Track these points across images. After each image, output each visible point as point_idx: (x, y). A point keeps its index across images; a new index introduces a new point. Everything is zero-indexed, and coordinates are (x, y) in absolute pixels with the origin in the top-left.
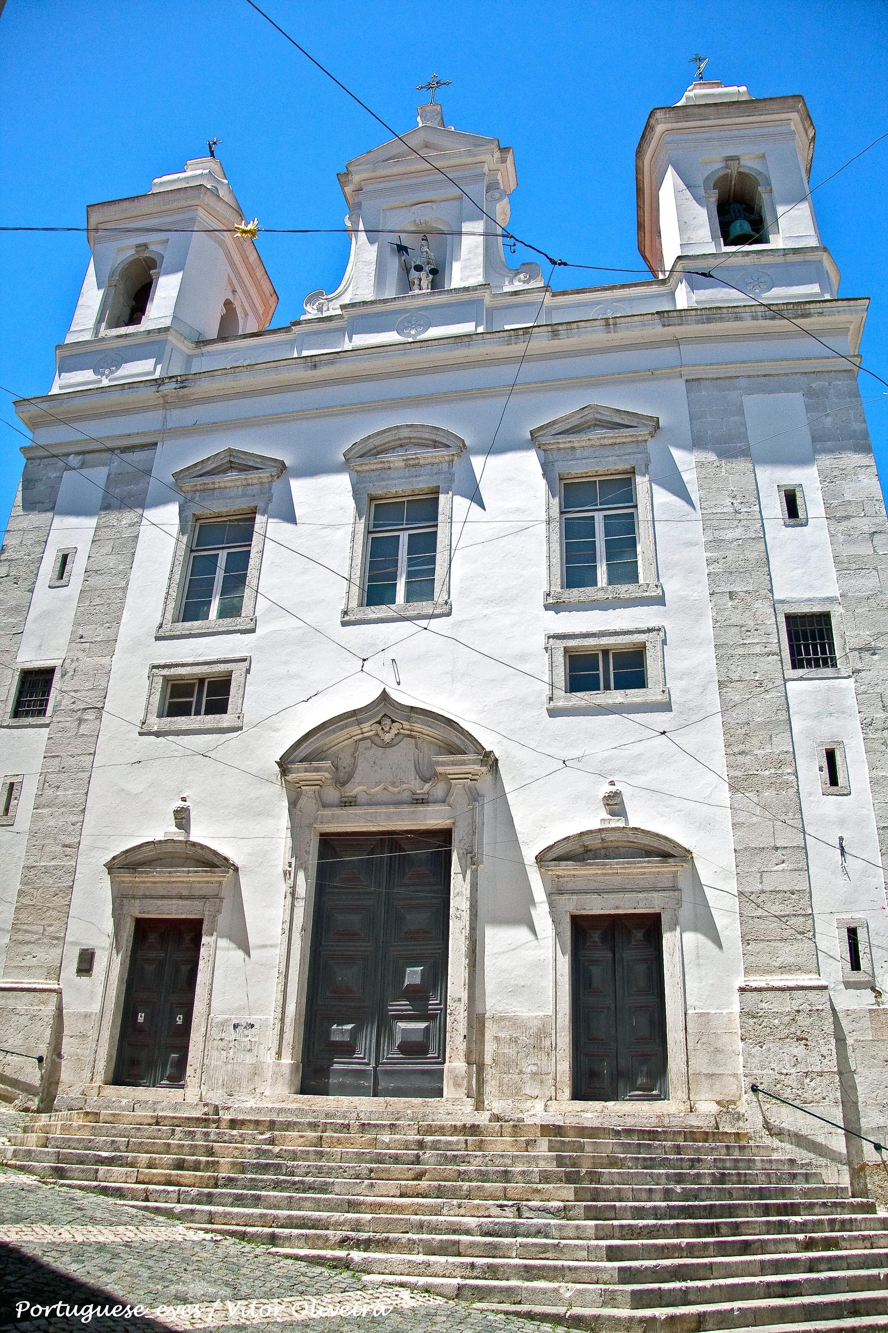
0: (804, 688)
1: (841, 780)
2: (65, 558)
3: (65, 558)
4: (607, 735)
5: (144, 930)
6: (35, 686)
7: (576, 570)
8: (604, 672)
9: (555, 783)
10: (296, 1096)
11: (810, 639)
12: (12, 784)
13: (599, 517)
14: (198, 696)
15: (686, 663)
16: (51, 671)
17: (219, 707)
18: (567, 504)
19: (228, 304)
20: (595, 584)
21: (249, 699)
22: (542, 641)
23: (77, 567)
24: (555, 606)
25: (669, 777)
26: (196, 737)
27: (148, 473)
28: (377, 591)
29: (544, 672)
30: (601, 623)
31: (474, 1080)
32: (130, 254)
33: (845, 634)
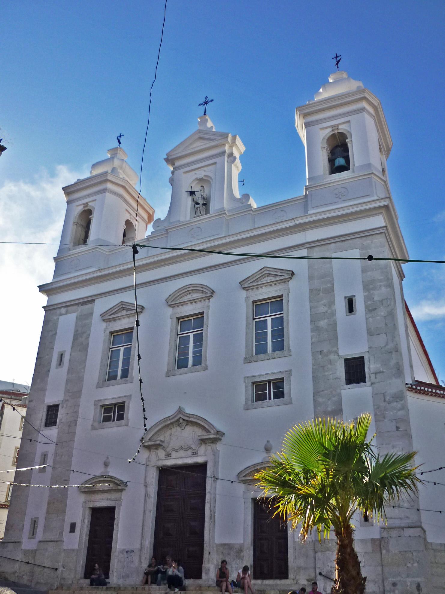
2: (62, 355)
3: (60, 364)
8: (271, 390)
13: (269, 320)
17: (121, 417)
26: (113, 429)
29: (243, 393)
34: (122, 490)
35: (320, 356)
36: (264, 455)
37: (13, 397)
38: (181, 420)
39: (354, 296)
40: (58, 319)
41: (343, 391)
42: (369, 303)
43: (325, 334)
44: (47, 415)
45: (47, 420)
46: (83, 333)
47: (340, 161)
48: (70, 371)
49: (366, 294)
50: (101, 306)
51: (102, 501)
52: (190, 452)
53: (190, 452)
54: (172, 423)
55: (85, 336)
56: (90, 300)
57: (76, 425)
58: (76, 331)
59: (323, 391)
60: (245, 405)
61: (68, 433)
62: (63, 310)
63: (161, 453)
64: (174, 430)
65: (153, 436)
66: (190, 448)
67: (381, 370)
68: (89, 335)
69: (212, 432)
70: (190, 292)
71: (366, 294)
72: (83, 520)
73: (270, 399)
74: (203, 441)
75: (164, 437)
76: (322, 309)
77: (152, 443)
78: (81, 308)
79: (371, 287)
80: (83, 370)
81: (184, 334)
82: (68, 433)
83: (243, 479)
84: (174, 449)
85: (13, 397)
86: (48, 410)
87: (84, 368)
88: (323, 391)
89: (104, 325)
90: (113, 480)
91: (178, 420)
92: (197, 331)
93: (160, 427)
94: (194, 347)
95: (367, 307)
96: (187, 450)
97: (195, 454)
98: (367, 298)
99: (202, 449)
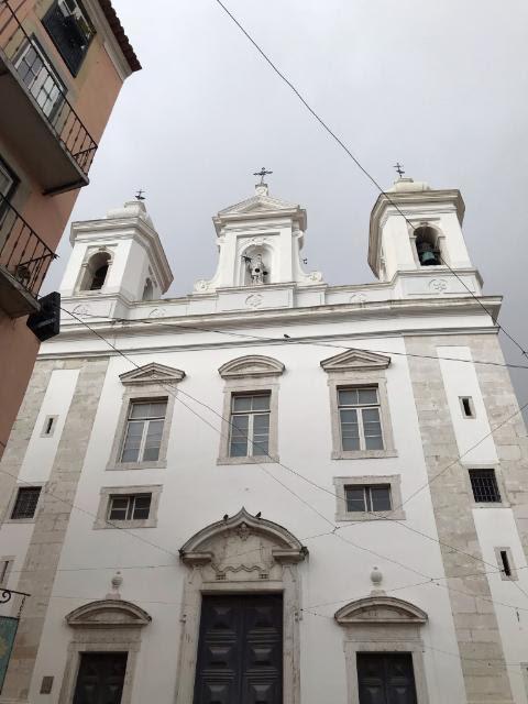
0: (483, 513)
1: (512, 572)
2: (51, 420)
3: (51, 420)
4: (370, 530)
5: (88, 659)
6: (26, 501)
7: (348, 441)
8: (369, 498)
9: (343, 566)
10: (91, 292)
11: (484, 485)
12: (7, 562)
13: (359, 411)
14: (131, 506)
15: (414, 495)
16: (39, 489)
18: (341, 400)
19: (148, 280)
20: (358, 449)
21: (161, 509)
22: (331, 480)
23: (58, 427)
24: (336, 457)
25: (401, 558)
26: (128, 535)
27: (104, 373)
28: (236, 448)
30: (365, 469)
31: (208, 536)
32: (96, 251)
33: (505, 482)
34: (142, 625)
35: (437, 463)
36: (373, 588)
37: (388, 307)
38: (244, 526)
39: (96, 527)
40: (51, 374)
41: (474, 510)
42: (491, 407)
43: (439, 440)
44: (17, 502)
45: (15, 508)
46: (87, 396)
47: (428, 256)
48: (64, 442)
49: (485, 396)
50: (120, 365)
51: (106, 643)
52: (255, 575)
53: (255, 575)
54: (229, 530)
55: (90, 400)
56: (104, 356)
57: (67, 519)
58: (78, 392)
59: (447, 506)
60: (337, 514)
61: (52, 530)
62: (60, 364)
63: (210, 574)
64: (230, 540)
65: (199, 545)
66: (258, 568)
67: (521, 488)
68: (98, 399)
69: (295, 547)
70: (254, 364)
71: (485, 396)
72: (67, 674)
73: (369, 510)
74: (279, 560)
75: (218, 549)
76: (431, 407)
77: (199, 556)
78: (85, 364)
79: (491, 390)
80: (84, 444)
81: (348, 406)
82: (52, 530)
83: (344, 620)
84: (230, 568)
85: (388, 307)
86: (19, 496)
87: (87, 441)
88: (447, 506)
89: (123, 389)
90: (128, 608)
91: (239, 526)
92: (368, 405)
93: (212, 533)
94: (256, 430)
95: (489, 412)
96: (250, 571)
97: (264, 577)
98: (487, 403)
99: (275, 572)
